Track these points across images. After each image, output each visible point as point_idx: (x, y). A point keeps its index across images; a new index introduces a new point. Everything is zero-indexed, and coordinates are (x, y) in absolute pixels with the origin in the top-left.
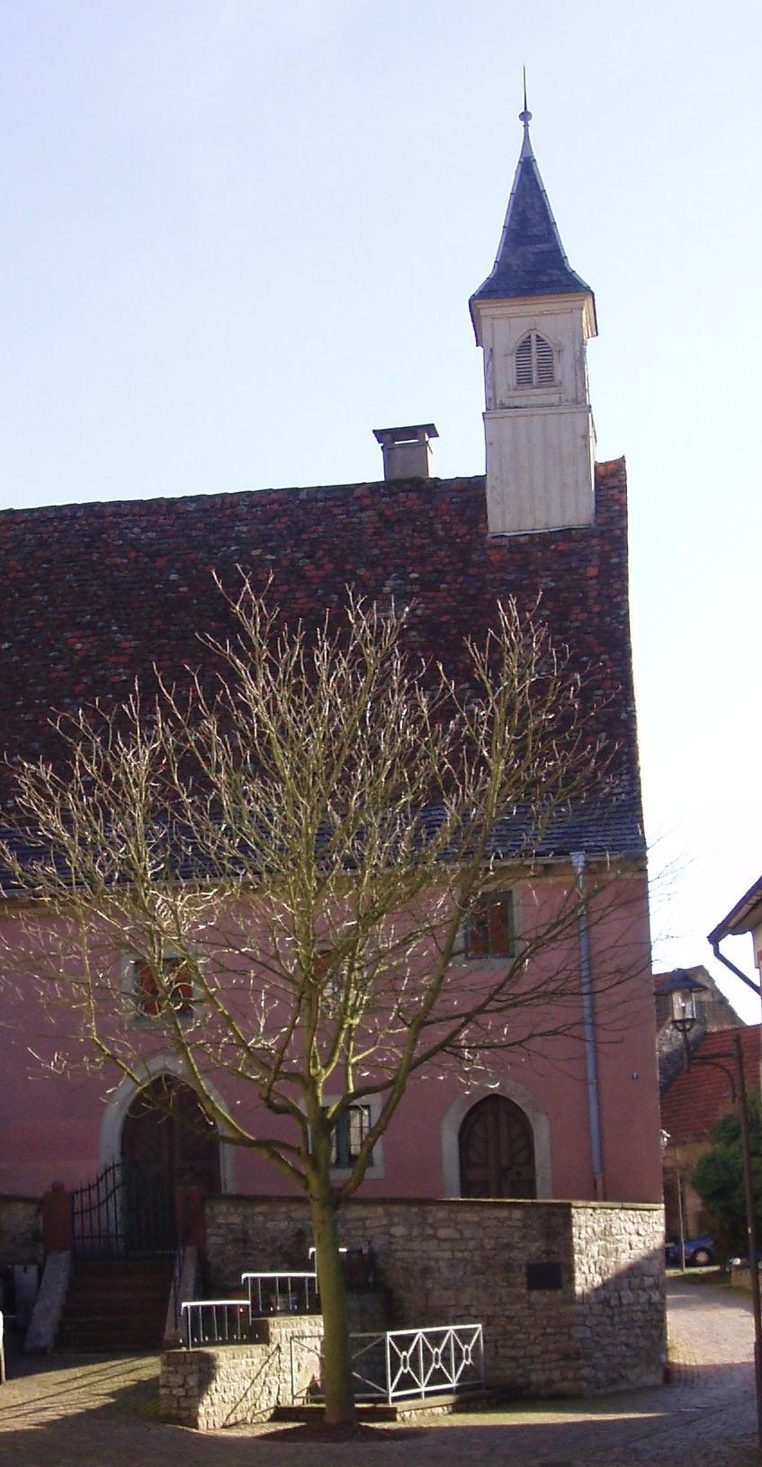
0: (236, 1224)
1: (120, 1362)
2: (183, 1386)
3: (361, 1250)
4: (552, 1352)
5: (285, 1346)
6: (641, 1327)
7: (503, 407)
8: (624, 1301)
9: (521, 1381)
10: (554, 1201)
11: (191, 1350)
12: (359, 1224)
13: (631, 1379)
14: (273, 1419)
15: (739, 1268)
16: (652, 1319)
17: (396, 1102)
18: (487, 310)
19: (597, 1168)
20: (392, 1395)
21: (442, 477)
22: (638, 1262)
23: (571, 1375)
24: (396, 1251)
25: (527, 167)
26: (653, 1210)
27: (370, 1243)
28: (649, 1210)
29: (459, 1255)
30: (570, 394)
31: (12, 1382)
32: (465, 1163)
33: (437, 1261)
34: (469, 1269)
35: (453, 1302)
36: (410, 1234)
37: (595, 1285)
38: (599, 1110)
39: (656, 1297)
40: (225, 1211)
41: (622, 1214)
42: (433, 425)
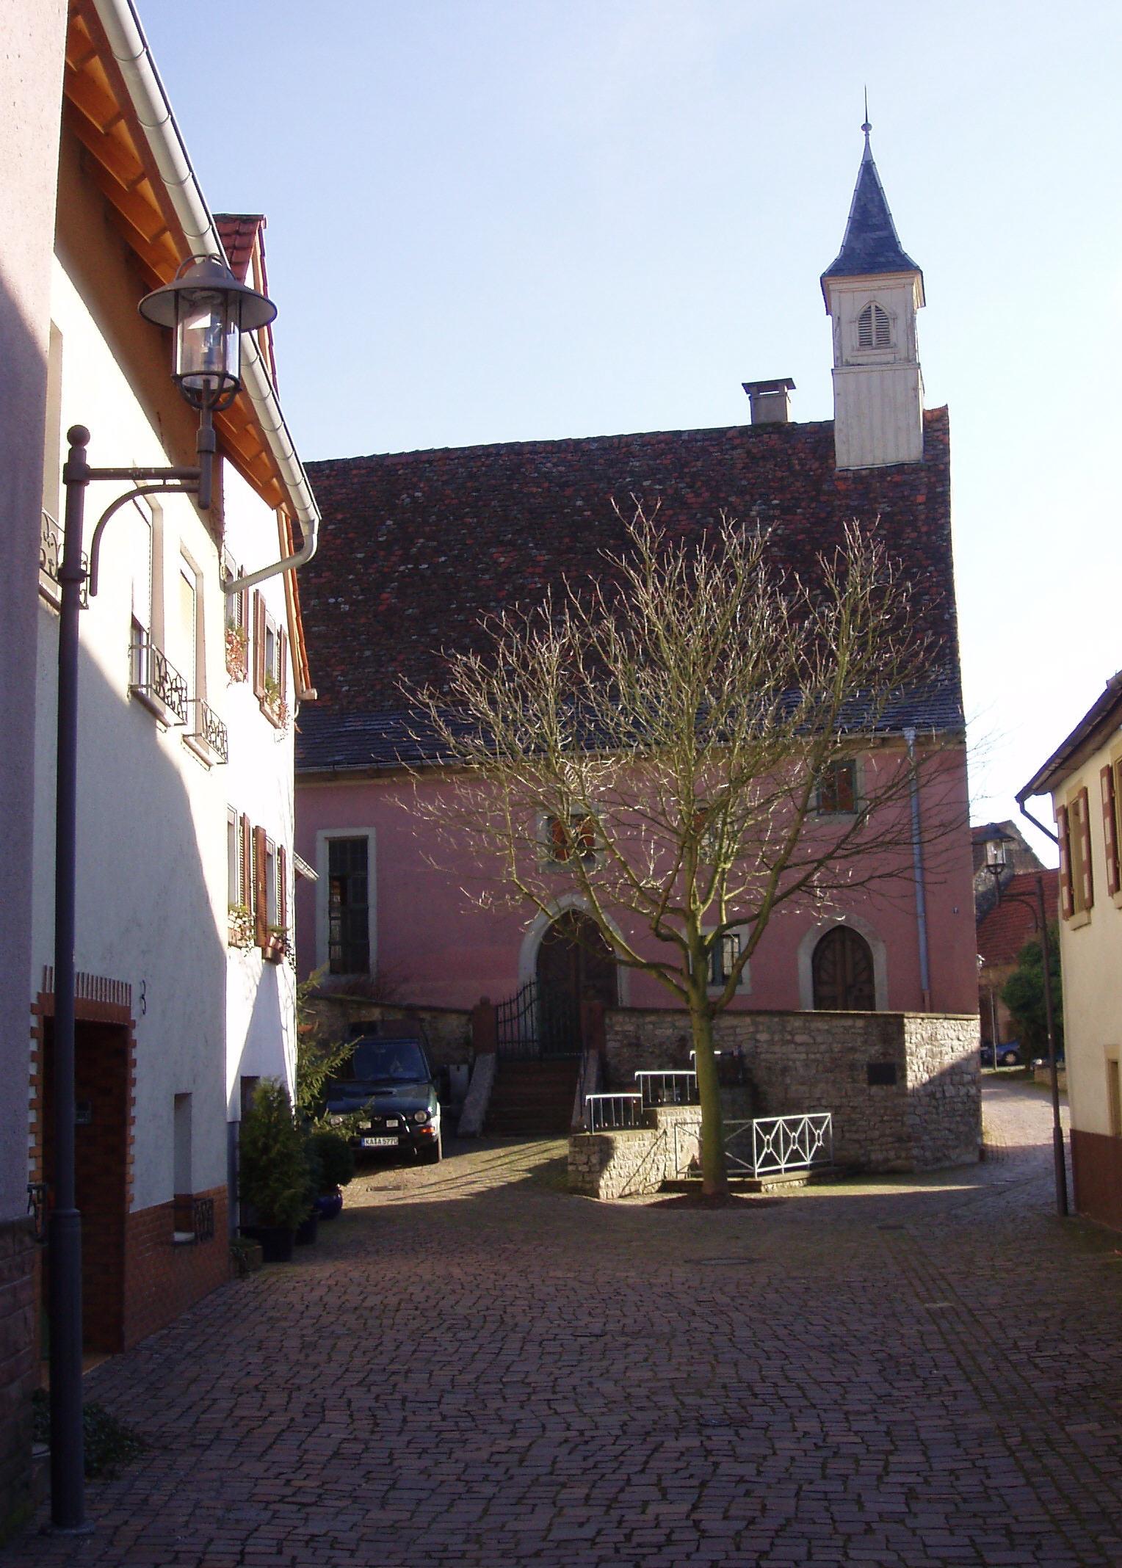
1: (535, 1144)
2: (587, 1163)
5: (670, 1131)
6: (961, 1116)
7: (849, 364)
8: (947, 1095)
9: (863, 1159)
10: (890, 1013)
11: (594, 1134)
15: (1040, 1066)
16: (970, 1109)
18: (835, 285)
19: (925, 986)
20: (757, 1170)
21: (799, 422)
23: (903, 1155)
24: (761, 1053)
25: (868, 169)
27: (740, 1046)
28: (967, 1020)
29: (812, 1056)
30: (903, 354)
33: (794, 1061)
34: (821, 1068)
35: (808, 1095)
36: (772, 1040)
37: (924, 1081)
40: (621, 1020)
41: (946, 1023)
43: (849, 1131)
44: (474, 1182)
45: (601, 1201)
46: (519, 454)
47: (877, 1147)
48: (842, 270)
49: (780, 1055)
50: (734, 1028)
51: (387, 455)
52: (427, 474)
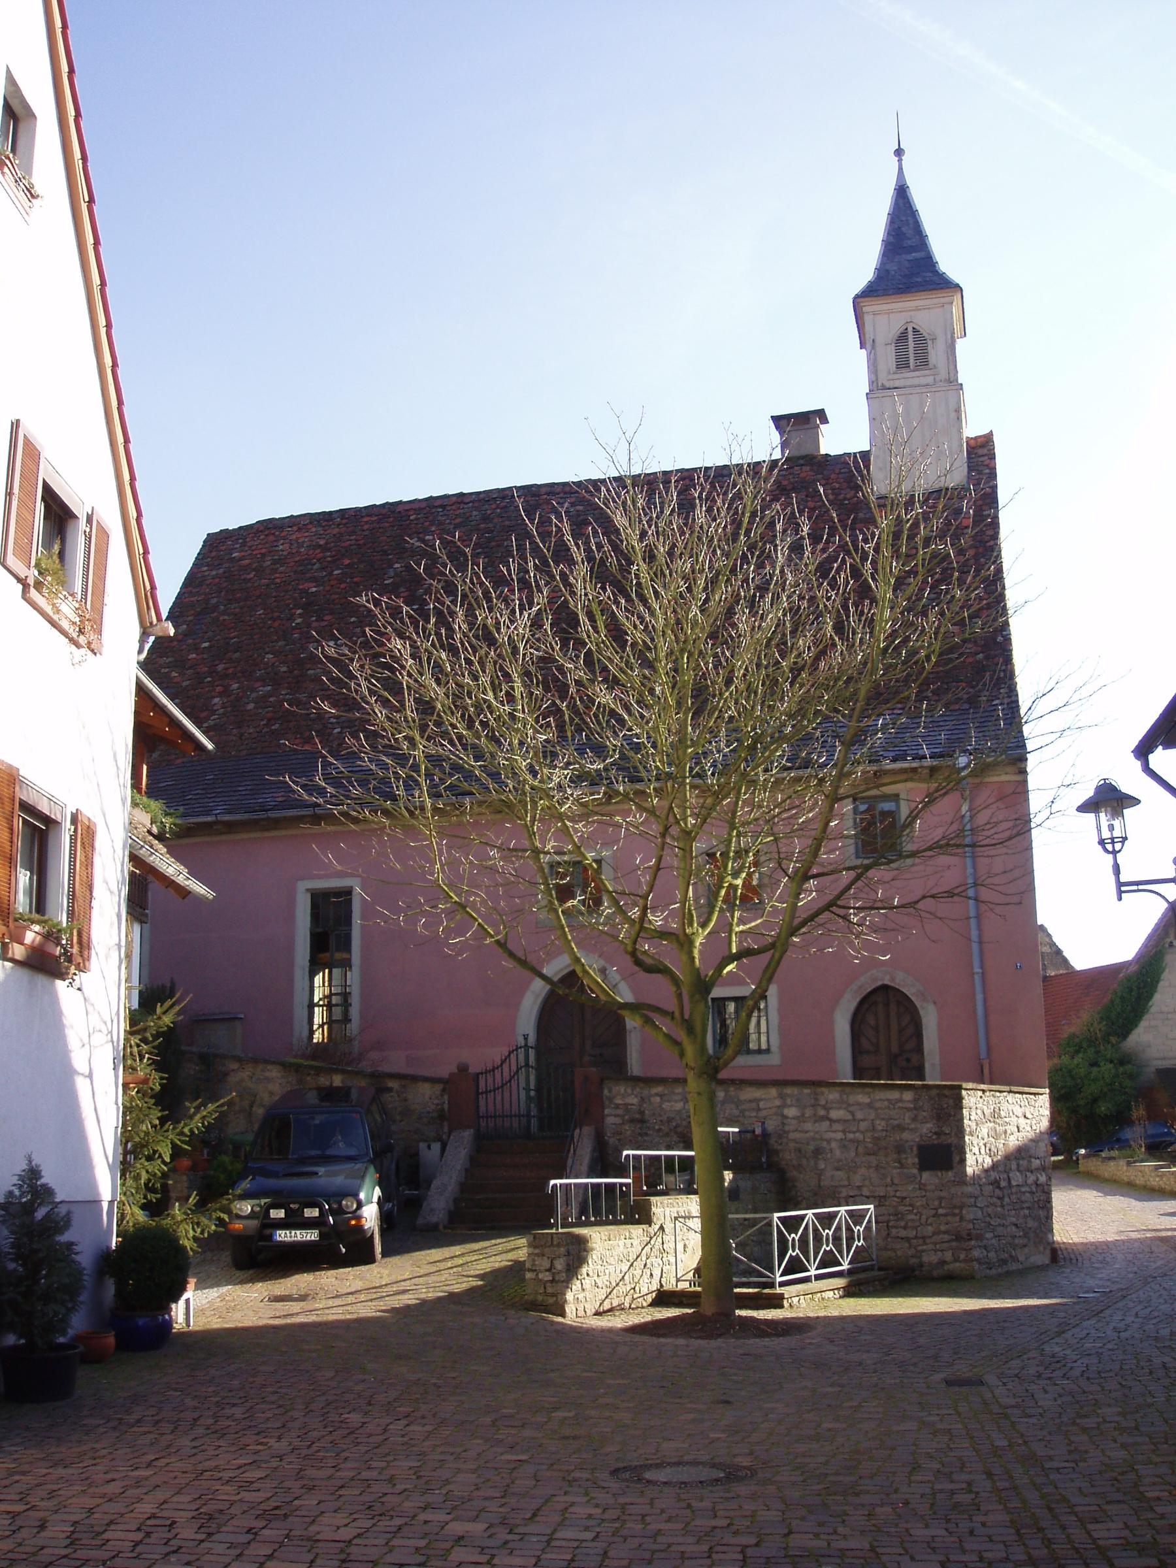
0: (632, 1105)
1: (504, 1240)
2: (549, 1270)
3: (754, 1132)
4: (945, 1233)
5: (669, 1227)
6: (1029, 1208)
7: (884, 388)
8: (1014, 1183)
9: (913, 1261)
10: (944, 1083)
11: (560, 1230)
12: (754, 1105)
13: (1020, 1259)
14: (654, 1304)
15: (1084, 1156)
16: (1039, 1200)
17: (778, 963)
18: (870, 307)
19: (983, 1055)
20: (779, 1279)
21: (832, 454)
22: (1025, 1145)
23: (962, 1256)
24: (788, 1132)
25: (902, 193)
26: (1038, 1094)
27: (763, 1123)
28: (1035, 1094)
29: (851, 1136)
30: (943, 374)
31: (388, 1259)
32: (857, 1050)
33: (829, 1141)
34: (861, 1149)
35: (846, 1183)
36: (803, 1115)
37: (985, 1166)
38: (985, 1001)
39: (1043, 1179)
40: (622, 1090)
41: (1010, 1097)
42: (823, 410)
43: (896, 1227)
44: (404, 1292)
45: (567, 1321)
46: (534, 495)
47: (930, 1247)
48: (877, 290)
49: (812, 1134)
50: (757, 1101)
51: (400, 502)
52: (440, 518)
